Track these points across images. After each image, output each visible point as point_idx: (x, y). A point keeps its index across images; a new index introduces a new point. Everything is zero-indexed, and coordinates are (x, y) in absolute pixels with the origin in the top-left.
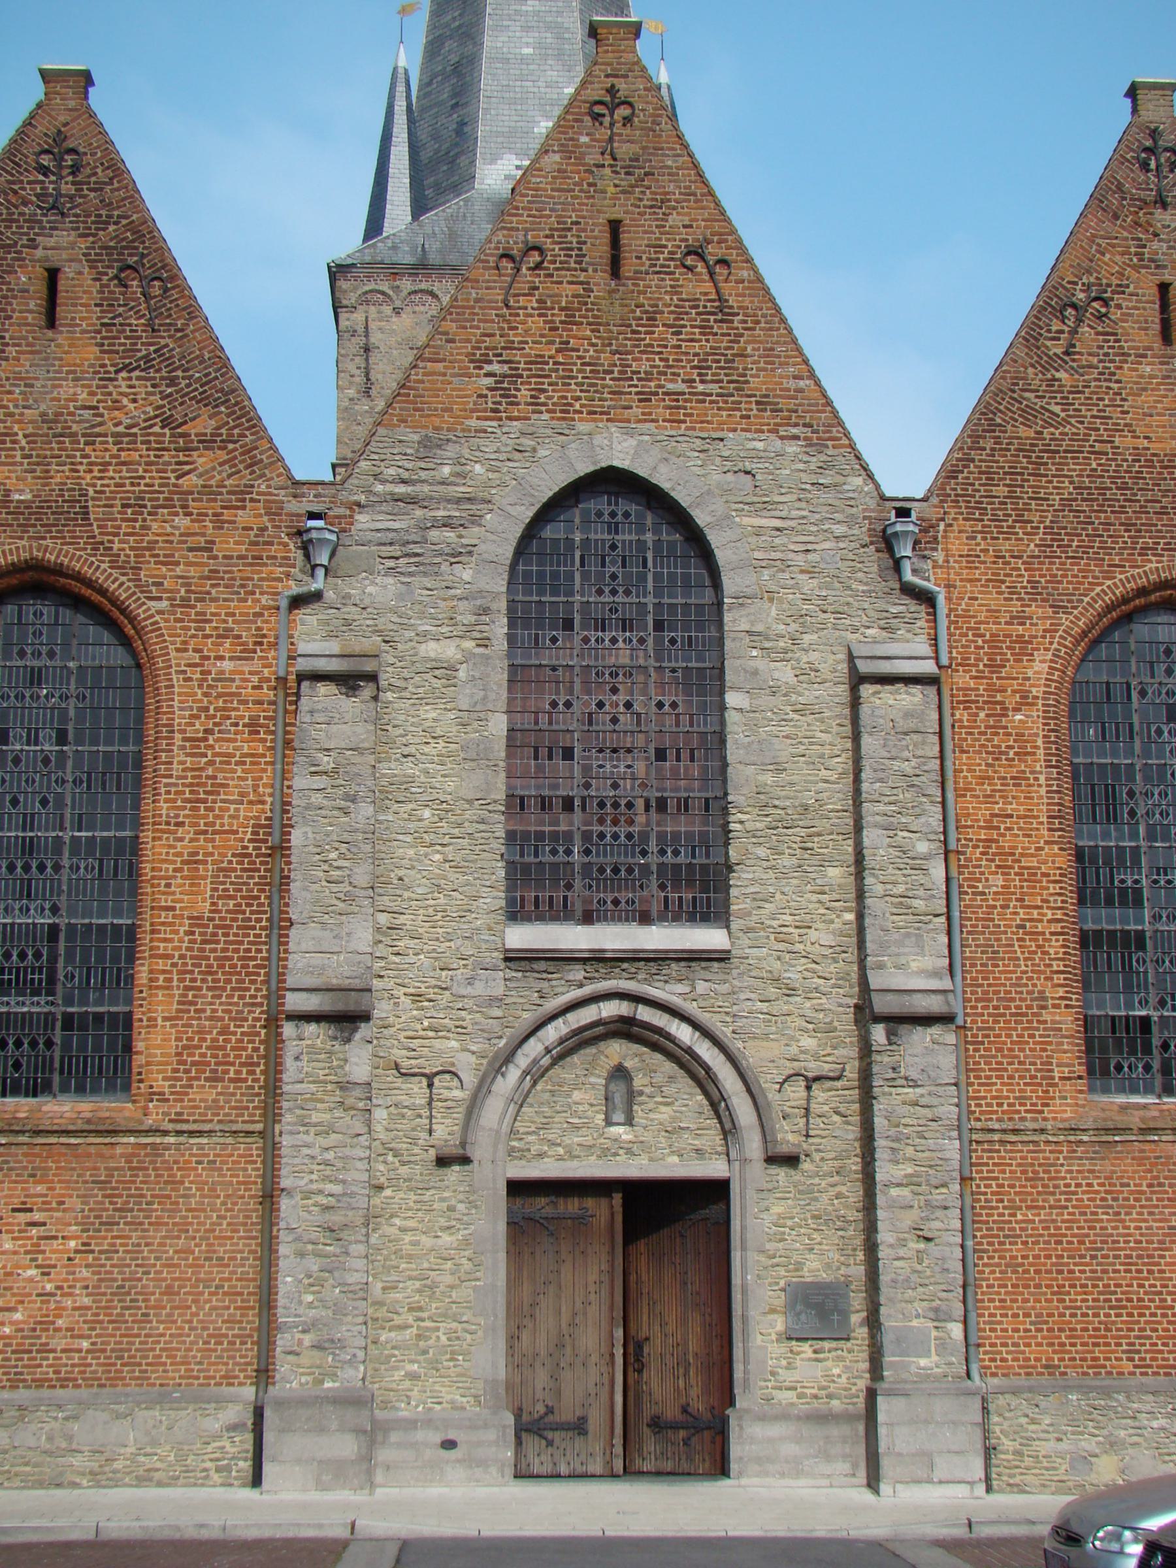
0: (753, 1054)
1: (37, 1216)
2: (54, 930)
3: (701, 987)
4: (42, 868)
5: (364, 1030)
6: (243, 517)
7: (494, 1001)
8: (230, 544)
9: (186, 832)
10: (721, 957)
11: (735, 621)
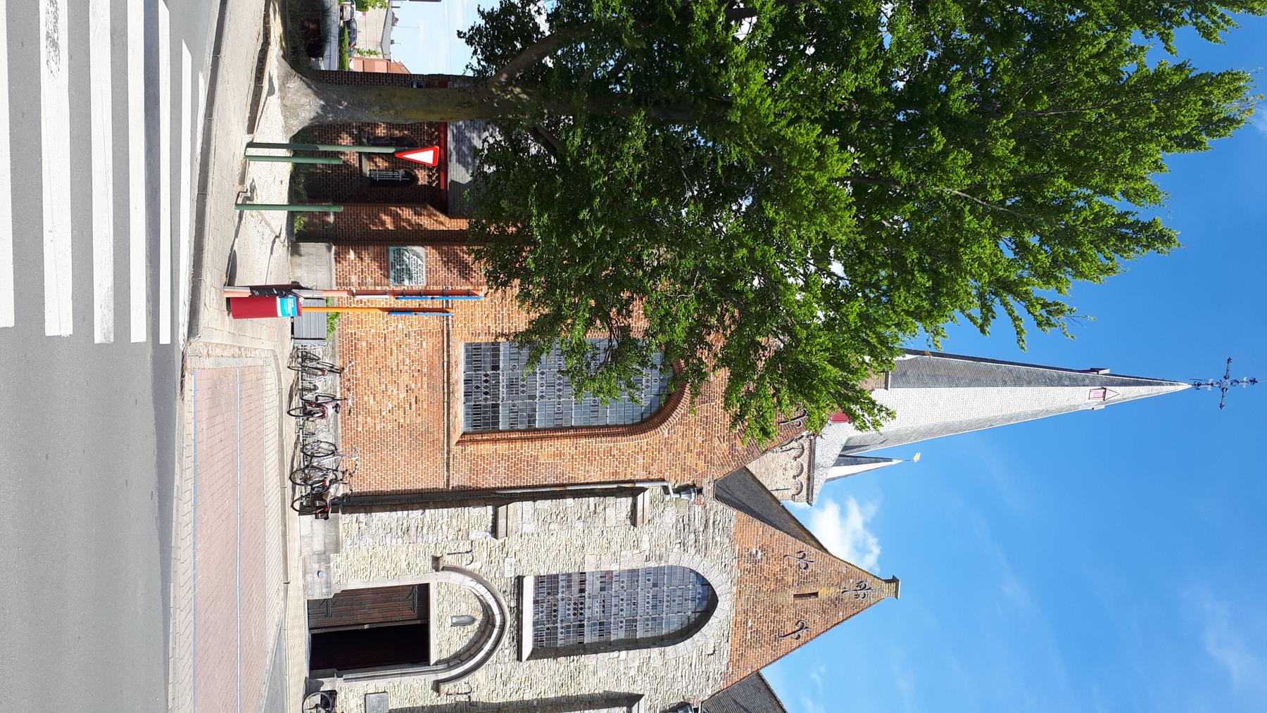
0: (480, 674)
1: (414, 406)
2: (533, 397)
3: (507, 652)
4: (559, 390)
5: (489, 536)
6: (701, 463)
8: (691, 460)
9: (573, 451)
10: (519, 658)
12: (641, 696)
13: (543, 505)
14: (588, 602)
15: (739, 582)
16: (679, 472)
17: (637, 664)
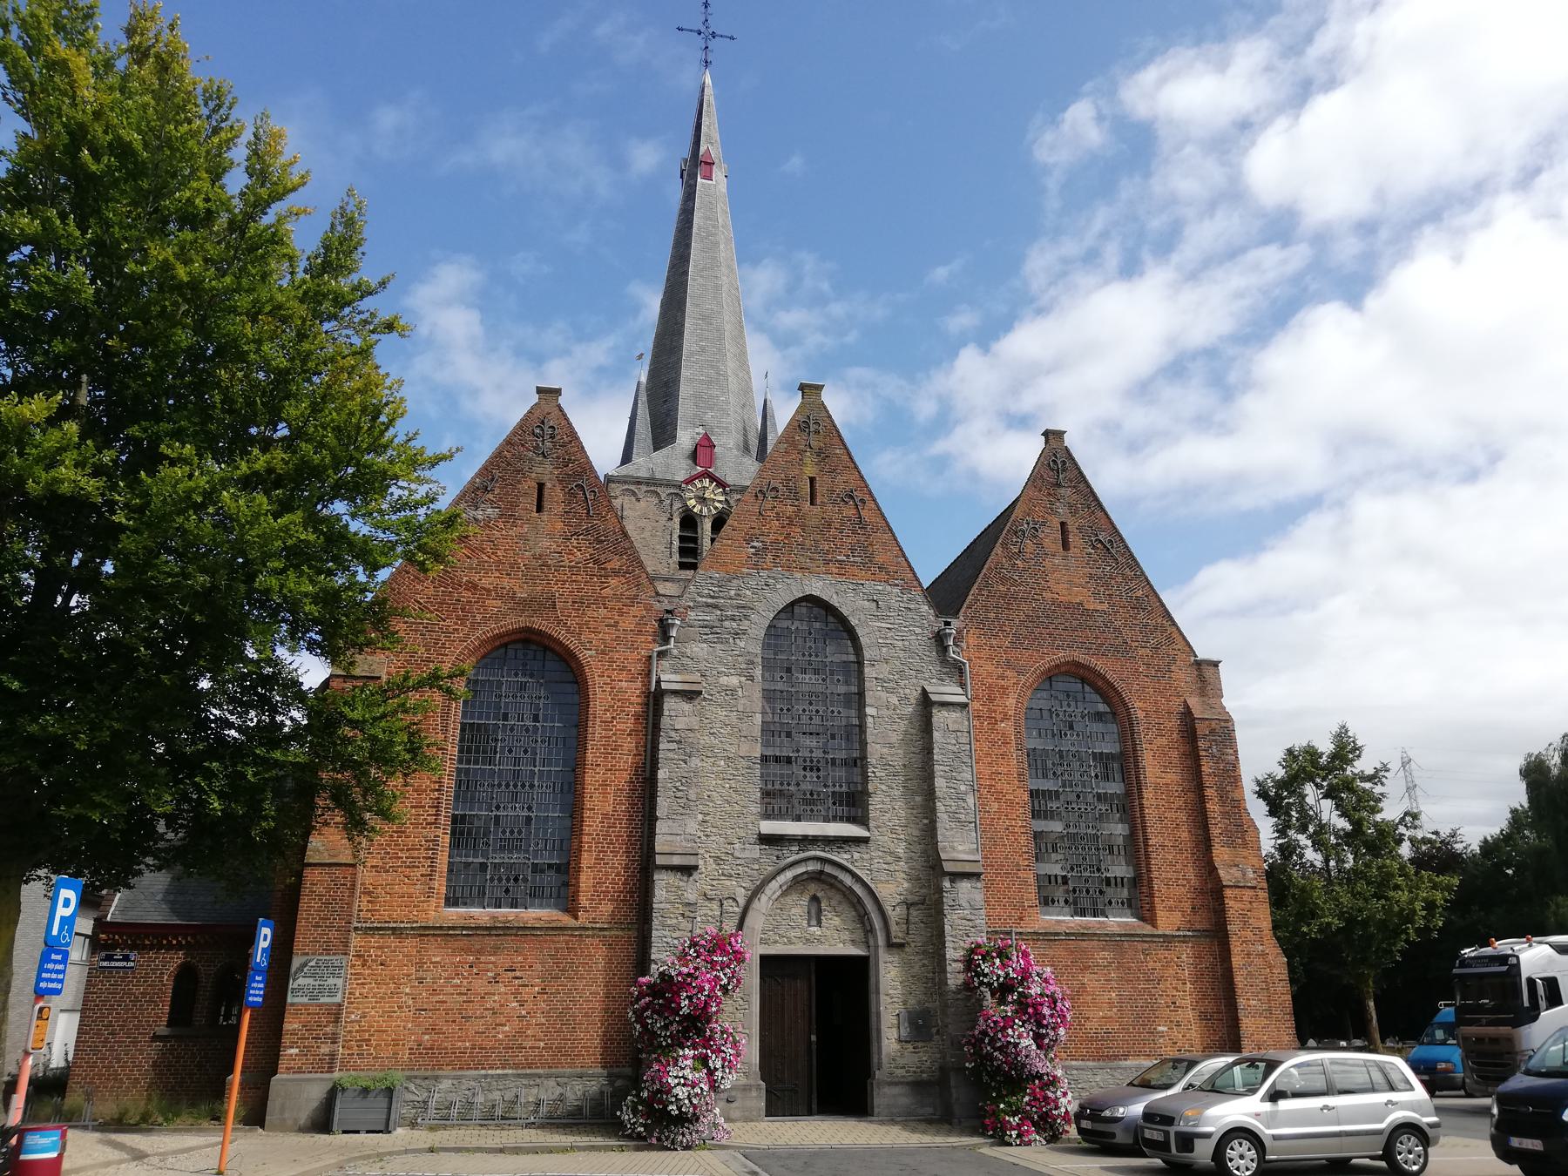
1: (518, 974)
2: (529, 819)
3: (856, 856)
4: (523, 786)
6: (634, 610)
7: (756, 860)
8: (628, 623)
10: (865, 840)
11: (868, 671)
12: (924, 689)
13: (663, 805)
14: (805, 753)
15: (789, 569)
16: (643, 638)
17: (884, 695)
